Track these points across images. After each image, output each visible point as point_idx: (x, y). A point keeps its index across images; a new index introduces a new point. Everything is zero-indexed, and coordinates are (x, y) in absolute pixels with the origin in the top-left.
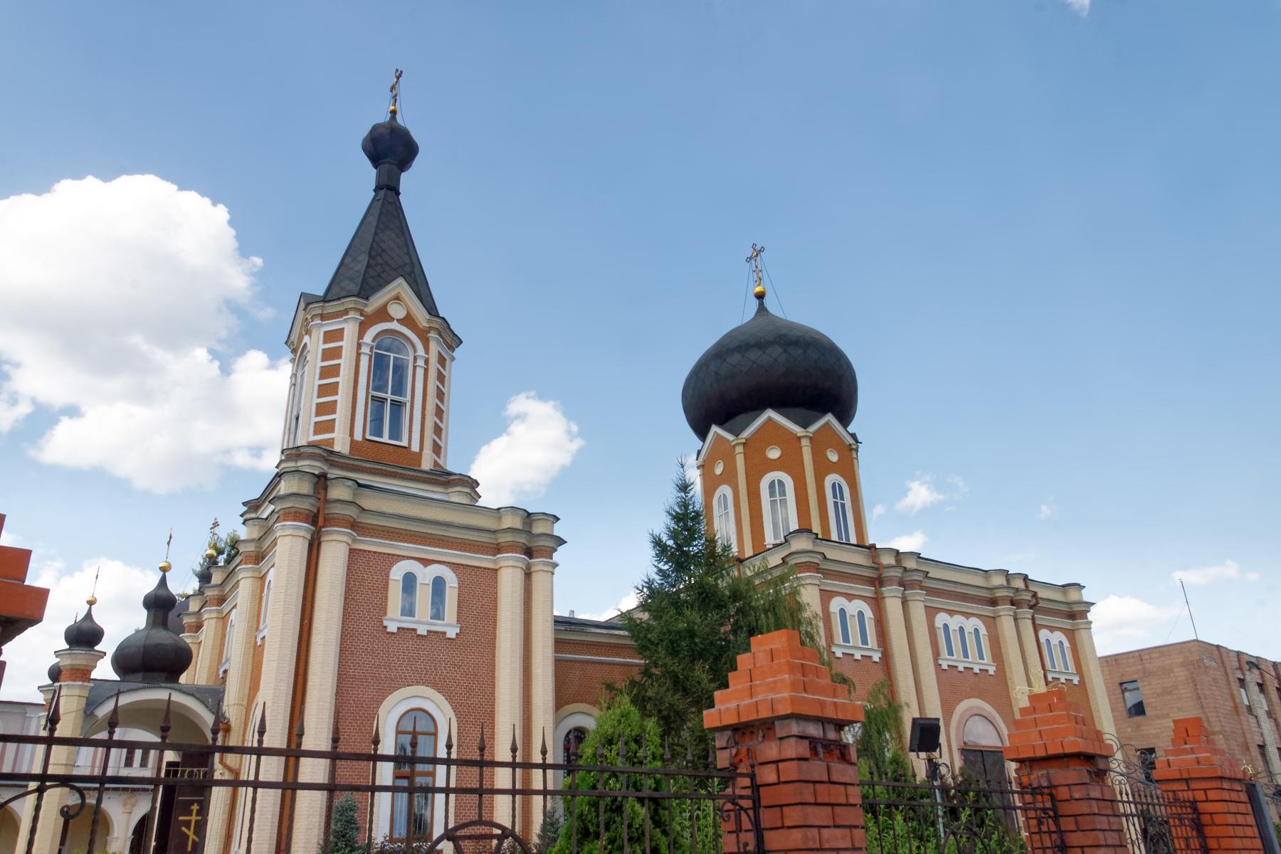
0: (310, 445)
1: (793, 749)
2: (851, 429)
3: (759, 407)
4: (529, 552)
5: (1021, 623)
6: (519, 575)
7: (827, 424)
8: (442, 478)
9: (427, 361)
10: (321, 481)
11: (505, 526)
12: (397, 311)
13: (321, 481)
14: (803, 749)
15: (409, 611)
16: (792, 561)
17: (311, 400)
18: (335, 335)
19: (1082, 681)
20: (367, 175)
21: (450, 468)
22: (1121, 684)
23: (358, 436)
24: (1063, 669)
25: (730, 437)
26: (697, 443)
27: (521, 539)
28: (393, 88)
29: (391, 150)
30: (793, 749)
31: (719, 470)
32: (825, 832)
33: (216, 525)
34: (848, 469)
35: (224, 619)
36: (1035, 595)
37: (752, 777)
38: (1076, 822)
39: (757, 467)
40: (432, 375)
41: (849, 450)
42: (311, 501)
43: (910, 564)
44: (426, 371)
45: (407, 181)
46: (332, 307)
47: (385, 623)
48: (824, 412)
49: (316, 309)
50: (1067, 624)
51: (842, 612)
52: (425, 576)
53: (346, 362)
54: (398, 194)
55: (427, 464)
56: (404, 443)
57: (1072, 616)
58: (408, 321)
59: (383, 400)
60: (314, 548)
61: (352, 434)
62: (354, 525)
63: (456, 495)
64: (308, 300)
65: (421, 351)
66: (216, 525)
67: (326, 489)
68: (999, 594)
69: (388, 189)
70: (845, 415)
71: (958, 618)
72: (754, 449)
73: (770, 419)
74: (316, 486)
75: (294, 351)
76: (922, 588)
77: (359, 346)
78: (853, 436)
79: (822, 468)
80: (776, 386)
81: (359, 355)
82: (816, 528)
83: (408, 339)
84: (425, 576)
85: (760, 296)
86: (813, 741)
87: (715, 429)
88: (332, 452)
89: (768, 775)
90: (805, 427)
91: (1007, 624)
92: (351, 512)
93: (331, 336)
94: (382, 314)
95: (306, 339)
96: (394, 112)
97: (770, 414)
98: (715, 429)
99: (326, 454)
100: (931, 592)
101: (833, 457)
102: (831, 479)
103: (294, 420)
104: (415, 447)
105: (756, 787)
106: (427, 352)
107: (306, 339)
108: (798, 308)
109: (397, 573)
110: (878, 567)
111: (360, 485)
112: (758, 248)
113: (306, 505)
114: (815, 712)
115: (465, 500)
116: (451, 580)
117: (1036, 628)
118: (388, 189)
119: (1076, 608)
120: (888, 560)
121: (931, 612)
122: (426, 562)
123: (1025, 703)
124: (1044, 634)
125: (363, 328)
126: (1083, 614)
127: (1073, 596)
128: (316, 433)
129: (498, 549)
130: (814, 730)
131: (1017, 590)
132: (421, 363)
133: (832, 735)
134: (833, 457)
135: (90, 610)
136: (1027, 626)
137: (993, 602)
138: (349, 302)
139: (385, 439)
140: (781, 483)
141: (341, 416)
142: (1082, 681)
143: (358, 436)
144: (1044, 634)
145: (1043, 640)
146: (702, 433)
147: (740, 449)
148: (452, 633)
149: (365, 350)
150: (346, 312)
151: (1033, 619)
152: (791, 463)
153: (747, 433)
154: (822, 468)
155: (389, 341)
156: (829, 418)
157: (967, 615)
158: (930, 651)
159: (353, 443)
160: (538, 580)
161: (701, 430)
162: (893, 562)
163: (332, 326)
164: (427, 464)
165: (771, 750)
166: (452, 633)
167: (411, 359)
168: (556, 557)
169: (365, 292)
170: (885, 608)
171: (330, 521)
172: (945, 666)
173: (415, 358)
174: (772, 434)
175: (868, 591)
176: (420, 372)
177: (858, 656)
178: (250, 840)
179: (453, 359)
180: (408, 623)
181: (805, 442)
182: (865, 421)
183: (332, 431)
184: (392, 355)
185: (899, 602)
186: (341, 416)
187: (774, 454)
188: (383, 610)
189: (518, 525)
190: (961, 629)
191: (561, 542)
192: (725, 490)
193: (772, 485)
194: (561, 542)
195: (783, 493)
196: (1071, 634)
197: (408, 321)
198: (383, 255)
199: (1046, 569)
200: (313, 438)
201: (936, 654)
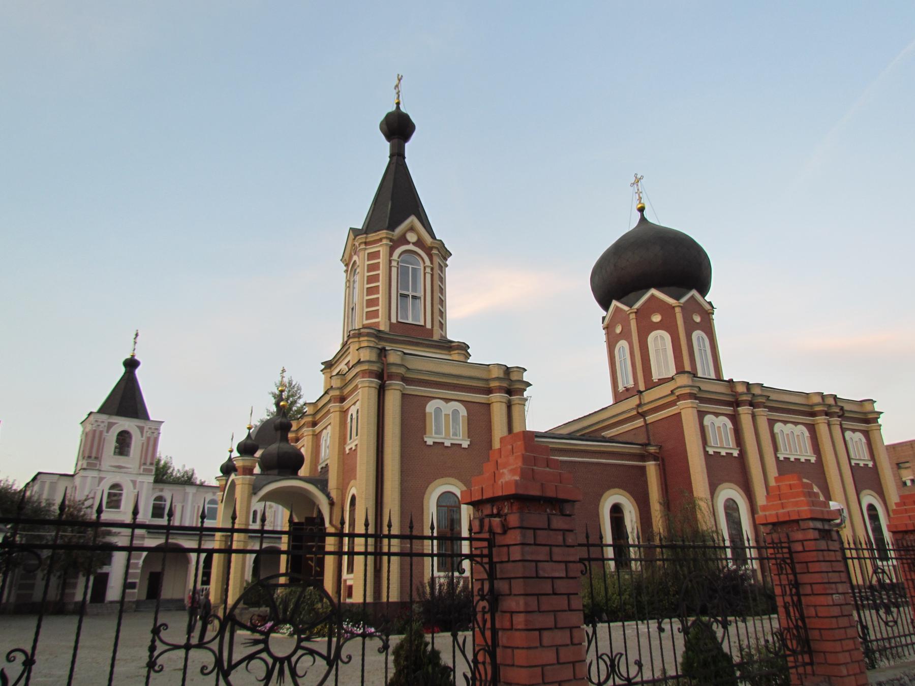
0: (364, 327)
1: (812, 534)
2: (708, 298)
3: (648, 288)
4: (509, 392)
5: (832, 427)
6: (504, 407)
7: (692, 297)
8: (447, 346)
9: (432, 269)
10: (382, 352)
11: (494, 376)
13: (382, 352)
14: (815, 534)
16: (678, 392)
17: (360, 297)
19: (875, 465)
20: (384, 147)
21: (449, 337)
22: (898, 464)
23: (394, 320)
24: (861, 455)
25: (626, 308)
26: (604, 313)
27: (505, 384)
28: (397, 86)
29: (398, 128)
30: (812, 534)
31: (618, 330)
32: (830, 574)
33: (284, 371)
34: (708, 328)
35: (317, 437)
36: (842, 408)
37: (789, 548)
38: (803, 545)
39: (645, 328)
40: (436, 277)
41: (707, 314)
42: (378, 365)
43: (757, 391)
44: (432, 275)
46: (372, 237)
47: (426, 439)
48: (690, 289)
49: (362, 238)
50: (863, 426)
53: (382, 272)
54: (404, 158)
56: (422, 323)
57: (867, 421)
58: (419, 243)
59: (407, 296)
61: (390, 319)
62: (404, 379)
63: (455, 355)
64: (355, 232)
65: (428, 263)
66: (284, 371)
67: (385, 357)
68: (817, 408)
69: (398, 156)
70: (704, 288)
71: (790, 426)
72: (643, 315)
73: (653, 296)
75: (347, 265)
76: (765, 407)
77: (390, 261)
78: (710, 303)
79: (690, 327)
80: (655, 274)
81: (390, 267)
82: (688, 368)
83: (419, 255)
85: (641, 210)
86: (819, 530)
87: (615, 303)
88: (380, 331)
89: (798, 547)
90: (677, 299)
91: (822, 429)
92: (401, 371)
94: (403, 240)
95: (355, 258)
96: (398, 104)
97: (653, 291)
98: (615, 303)
99: (378, 335)
100: (771, 409)
101: (697, 319)
102: (697, 335)
103: (350, 310)
104: (429, 326)
105: (790, 552)
106: (432, 263)
107: (355, 258)
108: (664, 217)
110: (736, 394)
111: (405, 354)
112: (639, 176)
113: (375, 368)
114: (820, 516)
115: (462, 358)
116: (463, 411)
117: (843, 430)
118: (398, 156)
119: (870, 416)
120: (741, 389)
121: (771, 423)
122: (447, 400)
123: (897, 500)
126: (875, 420)
127: (868, 407)
128: (367, 319)
129: (489, 391)
130: (819, 525)
131: (830, 406)
132: (428, 270)
133: (827, 527)
134: (697, 319)
135: (642, 215)
136: (837, 430)
137: (813, 414)
138: (383, 233)
139: (410, 321)
140: (662, 338)
141: (381, 308)
142: (875, 465)
143: (394, 320)
144: (848, 434)
145: (847, 438)
146: (605, 305)
147: (633, 316)
148: (465, 444)
149: (394, 264)
150: (381, 240)
151: (841, 425)
152: (668, 325)
153: (637, 305)
154: (690, 327)
156: (694, 292)
157: (796, 424)
158: (771, 445)
159: (391, 325)
160: (516, 410)
161: (605, 304)
162: (745, 390)
163: (372, 249)
165: (799, 536)
166: (465, 444)
168: (526, 394)
169: (392, 227)
170: (740, 422)
171: (391, 377)
172: (781, 458)
173: (425, 268)
175: (729, 410)
176: (428, 277)
177: (723, 453)
178: (411, 576)
179: (446, 266)
181: (677, 310)
182: (718, 294)
183: (377, 317)
184: (411, 266)
185: (750, 417)
186: (381, 308)
187: (657, 318)
189: (502, 376)
191: (529, 385)
194: (529, 385)
196: (866, 434)
197: (419, 243)
198: (398, 201)
199: (849, 390)
200: (365, 322)
201: (776, 449)
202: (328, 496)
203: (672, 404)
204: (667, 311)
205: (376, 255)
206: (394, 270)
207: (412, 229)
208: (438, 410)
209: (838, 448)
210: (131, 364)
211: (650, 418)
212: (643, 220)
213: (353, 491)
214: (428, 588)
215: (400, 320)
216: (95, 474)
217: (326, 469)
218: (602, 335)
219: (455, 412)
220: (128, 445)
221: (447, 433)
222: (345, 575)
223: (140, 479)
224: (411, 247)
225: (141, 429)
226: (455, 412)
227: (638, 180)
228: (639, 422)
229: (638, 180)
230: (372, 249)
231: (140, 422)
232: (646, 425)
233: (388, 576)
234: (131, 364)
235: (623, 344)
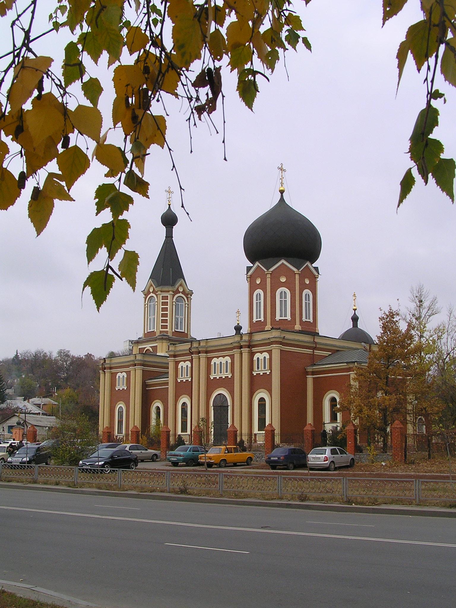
18: (166, 298)
20: (163, 229)
31: (258, 282)
45: (176, 229)
52: (185, 366)
62: (281, 343)
65: (187, 302)
69: (169, 236)
72: (275, 276)
73: (283, 264)
78: (316, 269)
85: (282, 192)
94: (177, 292)
97: (283, 261)
101: (307, 282)
104: (186, 332)
108: (301, 205)
118: (169, 236)
125: (174, 296)
134: (307, 282)
143: (173, 331)
147: (269, 276)
149: (174, 303)
150: (169, 292)
152: (290, 285)
153: (271, 270)
154: (303, 287)
156: (308, 263)
163: (165, 294)
174: (283, 270)
176: (187, 308)
181: (297, 277)
192: (259, 291)
193: (281, 293)
195: (286, 297)
204: (291, 275)
205: (166, 298)
206: (174, 306)
207: (181, 285)
209: (197, 369)
211: (317, 352)
212: (282, 200)
218: (246, 285)
224: (181, 295)
228: (310, 351)
230: (165, 294)
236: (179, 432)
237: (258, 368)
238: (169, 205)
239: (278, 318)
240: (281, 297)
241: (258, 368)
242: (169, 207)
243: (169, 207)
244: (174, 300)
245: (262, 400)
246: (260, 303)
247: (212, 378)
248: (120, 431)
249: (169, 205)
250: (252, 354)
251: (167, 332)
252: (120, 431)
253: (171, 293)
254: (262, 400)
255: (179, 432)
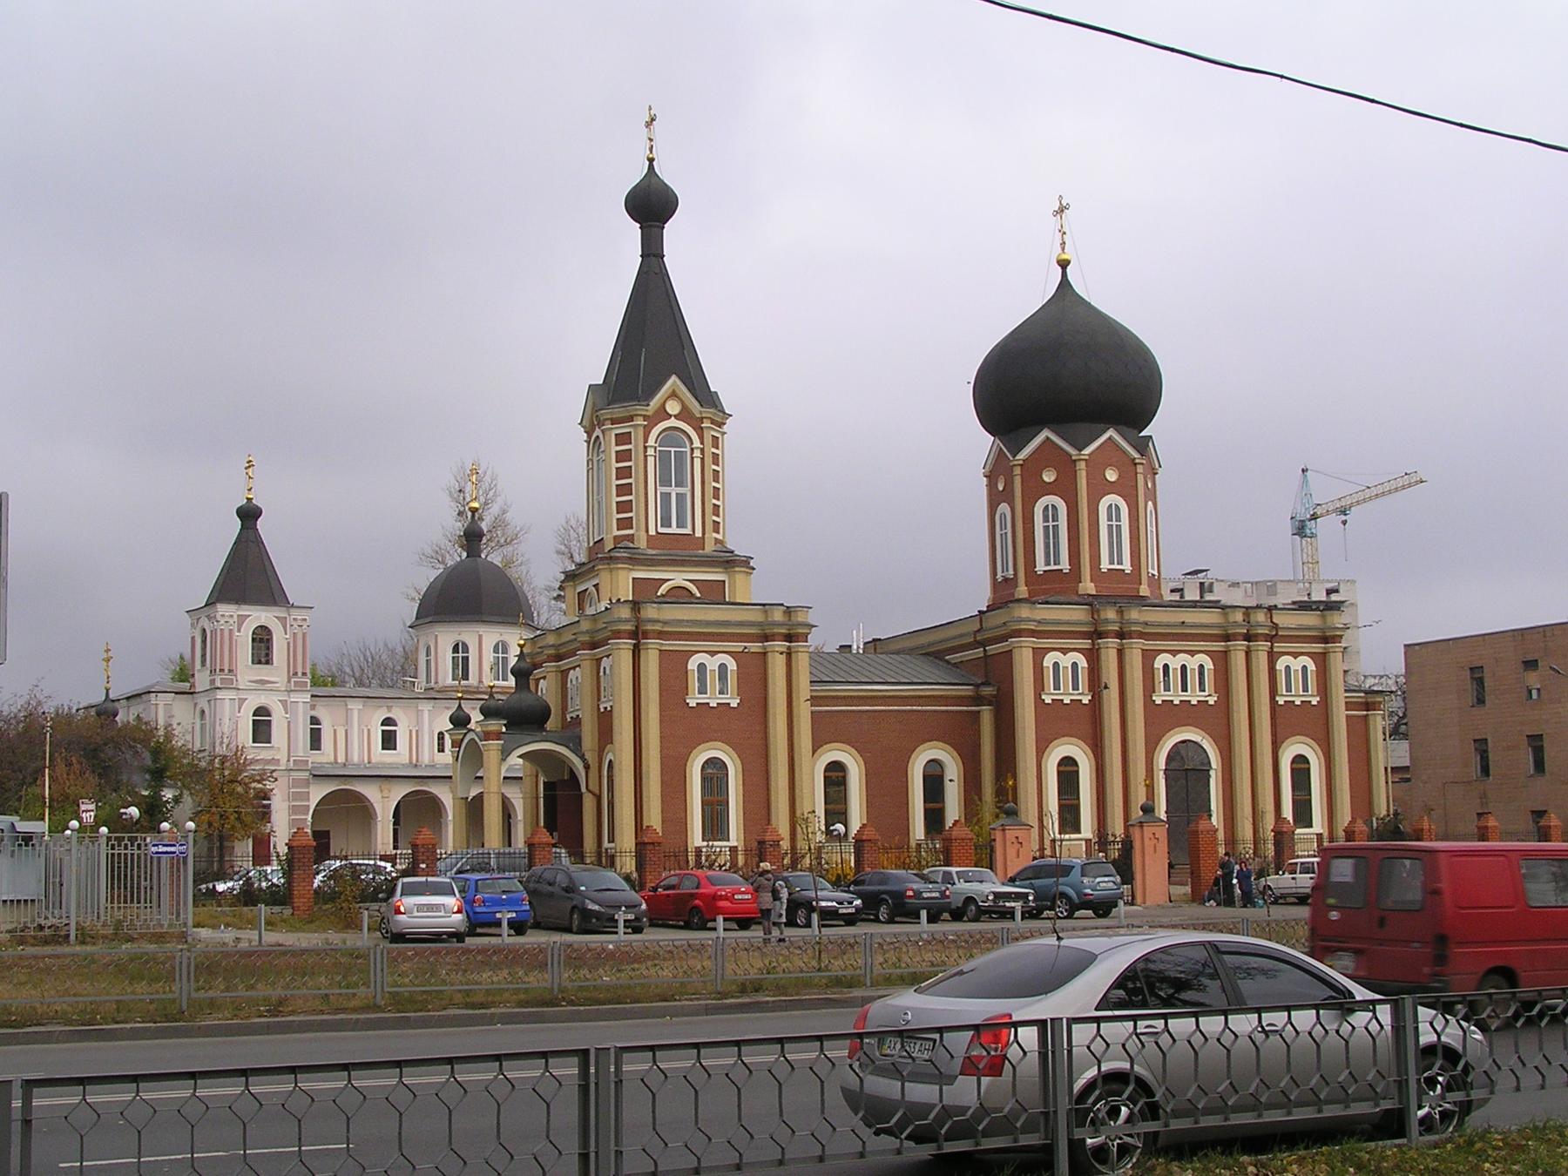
3: (1040, 423)
4: (789, 638)
9: (702, 450)
12: (673, 407)
15: (702, 691)
20: (635, 229)
23: (652, 532)
28: (649, 124)
29: (651, 206)
35: (639, 827)
39: (1036, 490)
44: (702, 459)
45: (670, 230)
50: (1317, 647)
51: (1056, 665)
55: (709, 548)
56: (688, 531)
57: (1325, 640)
60: (636, 652)
65: (697, 443)
69: (652, 252)
74: (633, 609)
84: (712, 663)
85: (1064, 264)
91: (1238, 660)
93: (623, 439)
94: (663, 414)
97: (1046, 433)
101: (1111, 475)
109: (693, 664)
116: (732, 665)
118: (652, 252)
122: (713, 653)
124: (1281, 664)
129: (766, 638)
132: (697, 453)
134: (1111, 475)
137: (1227, 638)
139: (674, 530)
143: (652, 532)
147: (1082, 465)
148: (734, 704)
149: (650, 451)
150: (631, 419)
155: (670, 436)
164: (709, 548)
166: (734, 704)
167: (688, 450)
171: (646, 635)
175: (1085, 643)
176: (697, 462)
180: (703, 699)
181: (1082, 465)
187: (1049, 477)
188: (685, 690)
190: (1184, 668)
202: (582, 757)
203: (1004, 638)
208: (702, 667)
210: (249, 514)
212: (1064, 284)
213: (610, 756)
214: (1271, 846)
215: (661, 530)
216: (232, 694)
217: (577, 721)
219: (723, 667)
220: (269, 648)
221: (713, 692)
222: (606, 844)
223: (294, 697)
224: (673, 422)
225: (283, 620)
226: (723, 667)
227: (1062, 210)
229: (1062, 210)
231: (280, 612)
232: (986, 656)
233: (597, 1124)
234: (249, 514)
235: (1004, 508)
236: (696, 838)
237: (1289, 689)
238: (651, 160)
239: (1041, 567)
240: (1046, 519)
241: (1289, 689)
242: (651, 167)
243: (651, 167)
244: (651, 442)
245: (1300, 762)
246: (1056, 528)
247: (1159, 702)
248: (715, 825)
249: (651, 160)
250: (1272, 657)
251: (631, 538)
252: (715, 825)
253: (640, 421)
254: (1300, 762)
255: (696, 838)
